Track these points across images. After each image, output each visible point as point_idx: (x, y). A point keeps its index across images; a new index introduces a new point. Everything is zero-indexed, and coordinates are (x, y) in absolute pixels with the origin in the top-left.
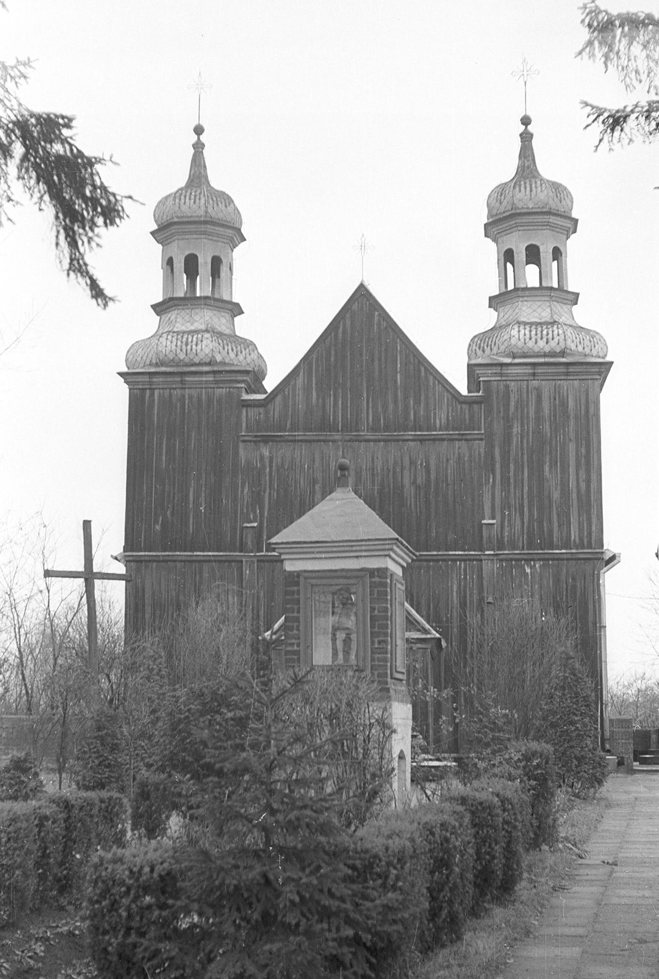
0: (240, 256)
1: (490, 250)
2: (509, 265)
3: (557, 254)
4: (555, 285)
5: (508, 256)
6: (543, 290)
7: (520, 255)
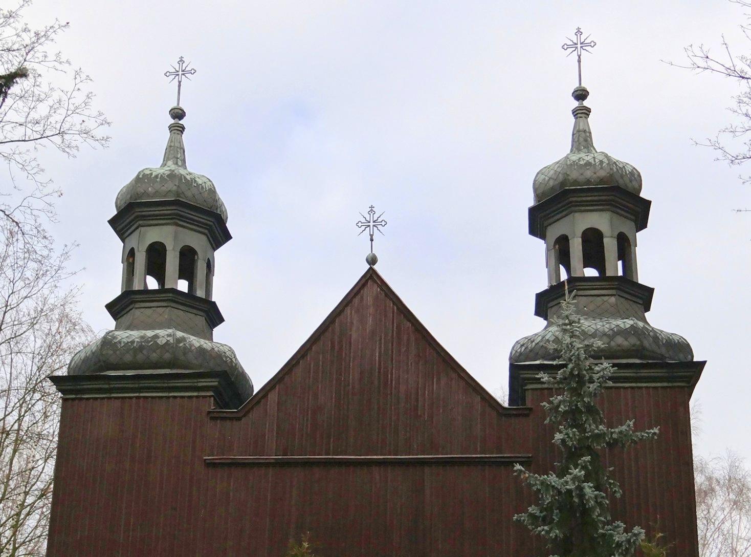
0: (221, 256)
4: (620, 273)
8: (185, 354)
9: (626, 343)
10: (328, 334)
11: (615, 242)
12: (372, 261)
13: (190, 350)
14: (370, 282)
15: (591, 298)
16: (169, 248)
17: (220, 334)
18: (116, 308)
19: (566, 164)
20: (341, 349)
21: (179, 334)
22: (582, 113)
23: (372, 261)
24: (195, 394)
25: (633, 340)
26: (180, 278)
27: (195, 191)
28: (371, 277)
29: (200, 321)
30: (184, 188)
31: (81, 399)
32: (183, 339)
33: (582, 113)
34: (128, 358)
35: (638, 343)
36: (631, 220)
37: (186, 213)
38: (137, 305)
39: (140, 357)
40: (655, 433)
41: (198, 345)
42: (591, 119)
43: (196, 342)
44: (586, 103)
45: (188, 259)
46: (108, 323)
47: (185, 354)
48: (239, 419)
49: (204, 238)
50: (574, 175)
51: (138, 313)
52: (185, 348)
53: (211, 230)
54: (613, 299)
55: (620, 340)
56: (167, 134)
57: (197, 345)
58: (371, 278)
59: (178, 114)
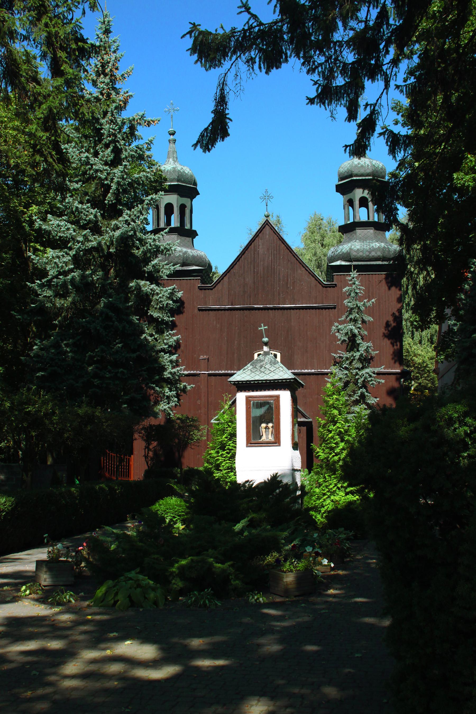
2: (350, 208)
5: (351, 203)
7: (357, 203)
9: (376, 255)
14: (267, 226)
20: (254, 257)
21: (184, 250)
28: (267, 224)
50: (356, 172)
58: (267, 223)
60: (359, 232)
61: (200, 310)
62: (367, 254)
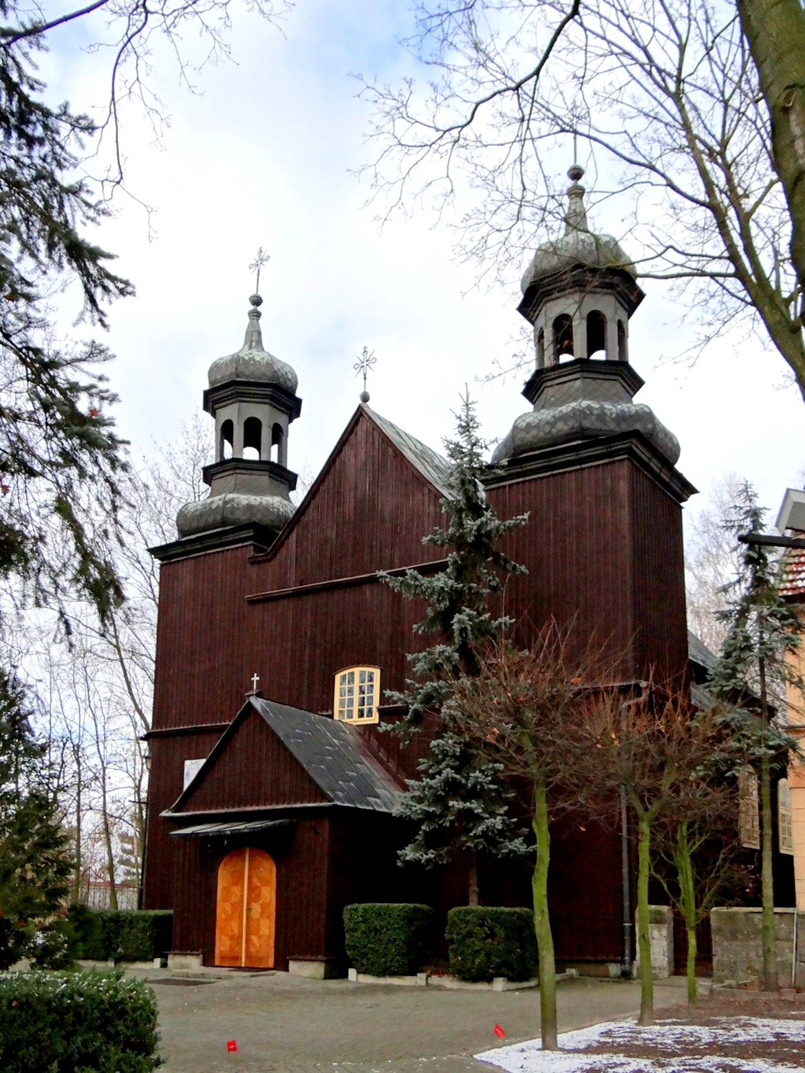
1: (209, 424)
3: (278, 435)
5: (226, 431)
6: (264, 466)
7: (239, 432)
8: (232, 513)
10: (330, 477)
11: (584, 323)
12: (365, 398)
13: (238, 508)
15: (557, 387)
16: (235, 423)
17: (640, 398)
18: (532, 390)
19: (236, 359)
22: (256, 315)
23: (365, 398)
24: (240, 545)
25: (571, 423)
26: (245, 446)
27: (252, 368)
29: (616, 387)
30: (241, 368)
31: (170, 563)
32: (233, 500)
33: (256, 315)
34: (195, 525)
35: (576, 425)
36: (610, 294)
37: (242, 389)
38: (218, 476)
39: (202, 523)
40: (524, 520)
41: (246, 502)
42: (261, 321)
43: (623, 407)
44: (259, 308)
45: (596, 324)
46: (527, 406)
47: (232, 513)
48: (270, 560)
49: (267, 407)
51: (549, 393)
52: (233, 507)
53: (271, 397)
54: (578, 383)
55: (560, 426)
56: (247, 320)
57: (245, 502)
58: (360, 415)
59: (257, 301)
60: (244, 477)
61: (252, 602)
62: (547, 428)
